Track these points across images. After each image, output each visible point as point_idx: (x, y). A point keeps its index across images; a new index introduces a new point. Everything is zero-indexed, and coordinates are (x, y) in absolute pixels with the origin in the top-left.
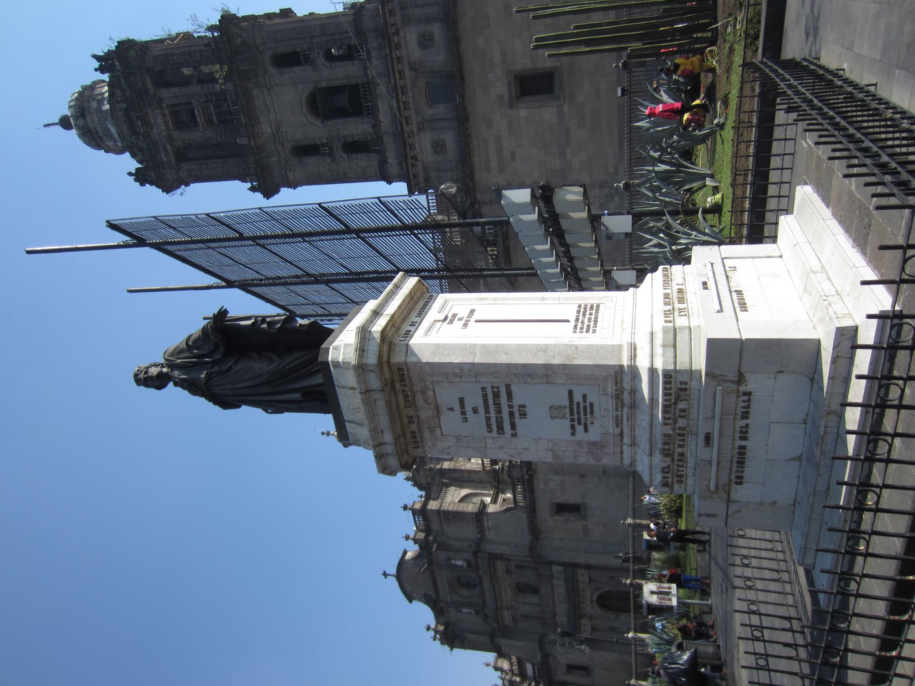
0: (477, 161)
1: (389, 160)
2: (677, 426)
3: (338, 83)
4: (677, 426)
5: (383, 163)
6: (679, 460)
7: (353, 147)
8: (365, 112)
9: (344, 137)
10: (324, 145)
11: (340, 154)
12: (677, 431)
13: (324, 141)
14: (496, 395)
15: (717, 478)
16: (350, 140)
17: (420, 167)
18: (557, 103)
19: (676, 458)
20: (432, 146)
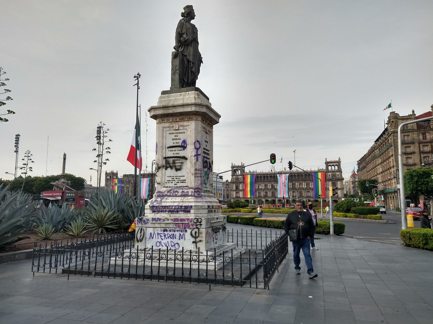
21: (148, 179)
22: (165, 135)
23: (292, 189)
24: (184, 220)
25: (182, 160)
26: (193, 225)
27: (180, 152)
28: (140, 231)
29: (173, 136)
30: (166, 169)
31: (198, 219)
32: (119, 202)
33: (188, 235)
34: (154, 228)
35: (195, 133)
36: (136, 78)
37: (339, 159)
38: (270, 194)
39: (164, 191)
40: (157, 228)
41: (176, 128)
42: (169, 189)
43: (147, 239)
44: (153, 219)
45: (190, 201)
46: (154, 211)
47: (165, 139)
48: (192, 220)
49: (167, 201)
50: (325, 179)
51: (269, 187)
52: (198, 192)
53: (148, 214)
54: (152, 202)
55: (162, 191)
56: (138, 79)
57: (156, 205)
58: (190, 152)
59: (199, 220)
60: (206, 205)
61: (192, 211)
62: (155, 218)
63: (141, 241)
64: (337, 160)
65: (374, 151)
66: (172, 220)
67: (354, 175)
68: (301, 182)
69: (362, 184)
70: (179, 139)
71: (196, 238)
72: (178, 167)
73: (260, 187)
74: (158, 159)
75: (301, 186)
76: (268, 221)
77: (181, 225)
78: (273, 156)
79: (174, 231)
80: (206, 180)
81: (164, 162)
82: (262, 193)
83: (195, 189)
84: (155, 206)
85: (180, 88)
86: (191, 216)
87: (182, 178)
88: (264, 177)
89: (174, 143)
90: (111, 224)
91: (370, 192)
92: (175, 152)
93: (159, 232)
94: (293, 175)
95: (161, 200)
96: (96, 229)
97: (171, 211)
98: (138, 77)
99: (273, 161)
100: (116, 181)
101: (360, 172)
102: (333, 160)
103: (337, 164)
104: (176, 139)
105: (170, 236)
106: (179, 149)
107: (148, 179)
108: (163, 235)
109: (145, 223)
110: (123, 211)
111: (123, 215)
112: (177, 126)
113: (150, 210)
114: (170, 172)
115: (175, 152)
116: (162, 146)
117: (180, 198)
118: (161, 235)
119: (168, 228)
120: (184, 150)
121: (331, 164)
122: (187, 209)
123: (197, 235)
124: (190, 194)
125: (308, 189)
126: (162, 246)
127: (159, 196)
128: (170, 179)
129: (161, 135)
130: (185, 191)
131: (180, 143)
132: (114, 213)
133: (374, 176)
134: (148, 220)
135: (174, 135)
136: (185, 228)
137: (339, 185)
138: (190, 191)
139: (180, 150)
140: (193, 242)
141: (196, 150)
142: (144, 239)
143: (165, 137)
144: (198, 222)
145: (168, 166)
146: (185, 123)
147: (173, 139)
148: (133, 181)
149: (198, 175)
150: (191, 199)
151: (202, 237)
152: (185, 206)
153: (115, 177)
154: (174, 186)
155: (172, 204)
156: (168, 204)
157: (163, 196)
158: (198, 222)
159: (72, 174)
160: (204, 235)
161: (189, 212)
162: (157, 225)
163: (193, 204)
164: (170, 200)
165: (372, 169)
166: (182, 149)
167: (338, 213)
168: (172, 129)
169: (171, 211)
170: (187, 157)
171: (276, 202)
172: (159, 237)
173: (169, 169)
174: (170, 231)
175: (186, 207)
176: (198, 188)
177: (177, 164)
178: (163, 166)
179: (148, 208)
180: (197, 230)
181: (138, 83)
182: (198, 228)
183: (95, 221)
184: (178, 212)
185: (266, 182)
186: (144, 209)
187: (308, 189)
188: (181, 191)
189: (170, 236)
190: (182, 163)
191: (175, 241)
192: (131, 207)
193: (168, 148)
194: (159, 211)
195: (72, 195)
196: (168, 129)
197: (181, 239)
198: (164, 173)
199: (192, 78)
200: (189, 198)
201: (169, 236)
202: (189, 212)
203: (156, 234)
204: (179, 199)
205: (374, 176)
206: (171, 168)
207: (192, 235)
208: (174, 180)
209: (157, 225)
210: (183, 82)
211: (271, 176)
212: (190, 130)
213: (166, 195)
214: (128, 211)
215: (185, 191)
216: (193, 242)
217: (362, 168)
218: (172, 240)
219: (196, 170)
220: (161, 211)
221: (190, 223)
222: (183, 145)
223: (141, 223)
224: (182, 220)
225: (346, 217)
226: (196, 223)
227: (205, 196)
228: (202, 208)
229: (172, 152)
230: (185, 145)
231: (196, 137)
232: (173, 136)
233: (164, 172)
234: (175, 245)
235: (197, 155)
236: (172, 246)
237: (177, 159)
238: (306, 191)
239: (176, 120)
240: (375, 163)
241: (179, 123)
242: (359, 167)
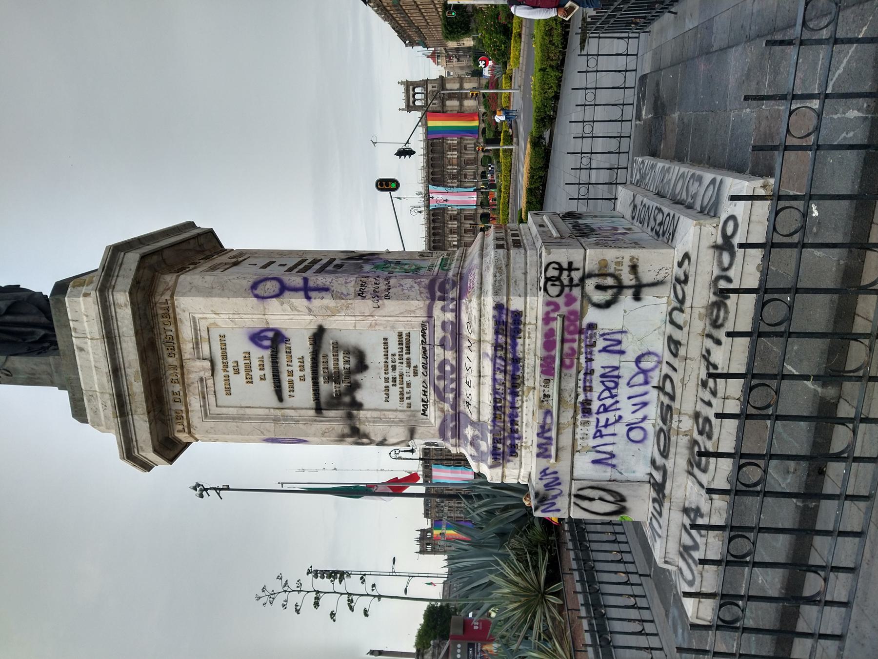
21: (434, 467)
22: (232, 411)
23: (460, 180)
24: (549, 337)
25: (327, 347)
26: (570, 300)
27: (296, 354)
28: (585, 504)
29: (238, 381)
30: (359, 406)
31: (547, 279)
32: (478, 545)
33: (606, 320)
34: (574, 451)
35: (220, 296)
36: (204, 493)
37: (402, 83)
38: (467, 225)
39: (438, 413)
40: (574, 440)
41: (204, 369)
42: (432, 396)
43: (616, 476)
44: (543, 453)
45: (478, 314)
46: (513, 451)
47: (248, 411)
48: (548, 304)
49: (474, 401)
50: (442, 113)
51: (454, 224)
52: (445, 288)
53: (523, 470)
54: (479, 459)
55: (438, 422)
56: (206, 490)
57: (490, 441)
58: (294, 317)
59: (552, 273)
60: (492, 253)
61: (516, 304)
62: (539, 446)
63: (623, 499)
64: (402, 88)
65: (385, 8)
66: (547, 381)
67: (434, 56)
68: (446, 161)
69: (451, 33)
70: (247, 356)
71: (620, 287)
72: (353, 361)
73: (456, 243)
74: (323, 434)
75: (455, 162)
76: (530, 183)
77: (567, 346)
78: (381, 185)
79: (590, 372)
80: (406, 267)
81: (332, 413)
82: (466, 239)
83: (433, 298)
84: (495, 448)
85: (59, 355)
86: (533, 307)
87: (394, 347)
88: (434, 234)
89: (263, 378)
90: (536, 567)
91: (468, 17)
92: (297, 373)
93: (592, 430)
94: (431, 176)
95: (473, 424)
96: (549, 608)
97: (514, 386)
98: (201, 490)
99: (393, 185)
100: (436, 532)
101: (428, 41)
102: (403, 96)
103: (411, 87)
104: (248, 368)
105: (608, 389)
106: (283, 357)
107: (434, 467)
108: (603, 418)
109: (557, 481)
110: (502, 535)
111: (513, 537)
112: (199, 364)
113: (509, 465)
114: (371, 391)
115: (297, 373)
116: (276, 420)
117: (466, 353)
118: (602, 423)
119: (577, 396)
120: (285, 340)
121: (411, 99)
122: (509, 325)
123: (610, 281)
124: (450, 316)
125: (461, 148)
126: (644, 419)
127: (457, 433)
128: (395, 391)
129: (232, 425)
130: (439, 334)
131: (259, 354)
132: (505, 558)
133: (436, 9)
134: (544, 472)
135: (234, 378)
136: (581, 332)
137: (452, 86)
138: (442, 316)
139: (289, 353)
140: (637, 297)
141: (287, 293)
142: (613, 487)
143: (241, 411)
144: (558, 279)
145: (347, 399)
146: (187, 332)
147: (250, 381)
148: (437, 499)
149: (383, 286)
150: (470, 309)
151: (619, 263)
152: (497, 332)
153: (429, 534)
154: (420, 377)
155: (488, 381)
156: (487, 398)
157: (457, 416)
158: (558, 279)
159: (416, 633)
160: (610, 254)
161: (517, 316)
162: (566, 440)
163: (489, 302)
164: (473, 391)
165: (422, 13)
166: (283, 348)
167: (512, 55)
168: (210, 382)
169: (514, 386)
170: (313, 327)
171: (485, 211)
172: (610, 430)
173: (360, 396)
174: (588, 389)
175: (500, 327)
176: (431, 287)
177: (341, 365)
178: (350, 416)
179: (499, 470)
180: (590, 284)
181: (215, 489)
182: (582, 280)
183: (529, 609)
184: (516, 361)
185: (444, 231)
186: (503, 486)
187: (461, 148)
188: (438, 350)
189: (608, 389)
190: (336, 346)
191: (628, 369)
192: (491, 513)
193: (280, 399)
194: (513, 431)
195: (459, 651)
196: (211, 399)
197: (623, 347)
198: (376, 414)
199: (35, 310)
200: (464, 318)
201: (606, 394)
202: (517, 316)
203: (599, 441)
204: (469, 358)
205: (436, 9)
206: (354, 387)
207: (607, 305)
208: (401, 375)
209: (566, 440)
210: (46, 345)
211: (434, 221)
212: (210, 314)
213: (455, 405)
214: (502, 521)
215: (439, 334)
216: (637, 297)
217: (420, 37)
218: (623, 382)
219: (361, 295)
220: (513, 422)
221: (564, 310)
222: (267, 343)
223: (555, 497)
224: (549, 344)
225: (520, 35)
226: (563, 286)
227: (461, 267)
228: (503, 271)
229: (297, 384)
230: (271, 334)
231: (236, 294)
232: (238, 381)
233: (369, 414)
234: (644, 372)
235: (307, 291)
236: (646, 383)
237: (321, 367)
238: (464, 151)
239: (175, 367)
240: (408, 7)
241: (186, 356)
242: (418, 44)
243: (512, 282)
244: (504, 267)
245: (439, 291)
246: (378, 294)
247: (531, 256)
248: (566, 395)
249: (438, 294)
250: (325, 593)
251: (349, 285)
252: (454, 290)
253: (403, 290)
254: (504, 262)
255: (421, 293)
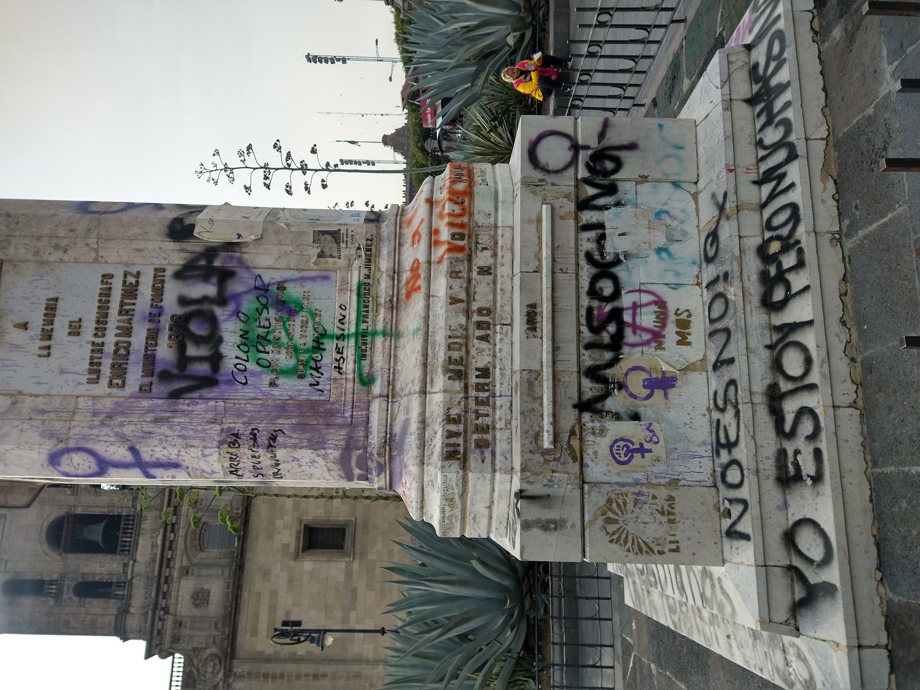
0: (244, 620)
1: (132, 610)
2: (475, 306)
3: (97, 511)
4: (475, 306)
5: (124, 611)
6: (479, 387)
7: (90, 589)
8: (119, 548)
9: (84, 574)
10: (51, 582)
11: (68, 594)
12: (476, 318)
13: (55, 577)
14: (131, 291)
15: (555, 423)
16: (90, 579)
17: (170, 620)
18: (347, 559)
19: (473, 380)
20: (192, 597)
243: (469, 518)
244: (457, 497)
245: (358, 466)
246: (262, 472)
247: (501, 483)
248: (565, 378)
249: (357, 472)
250: (277, 169)
251: (211, 459)
252: (382, 476)
253: (300, 466)
254: (457, 491)
255: (329, 470)
